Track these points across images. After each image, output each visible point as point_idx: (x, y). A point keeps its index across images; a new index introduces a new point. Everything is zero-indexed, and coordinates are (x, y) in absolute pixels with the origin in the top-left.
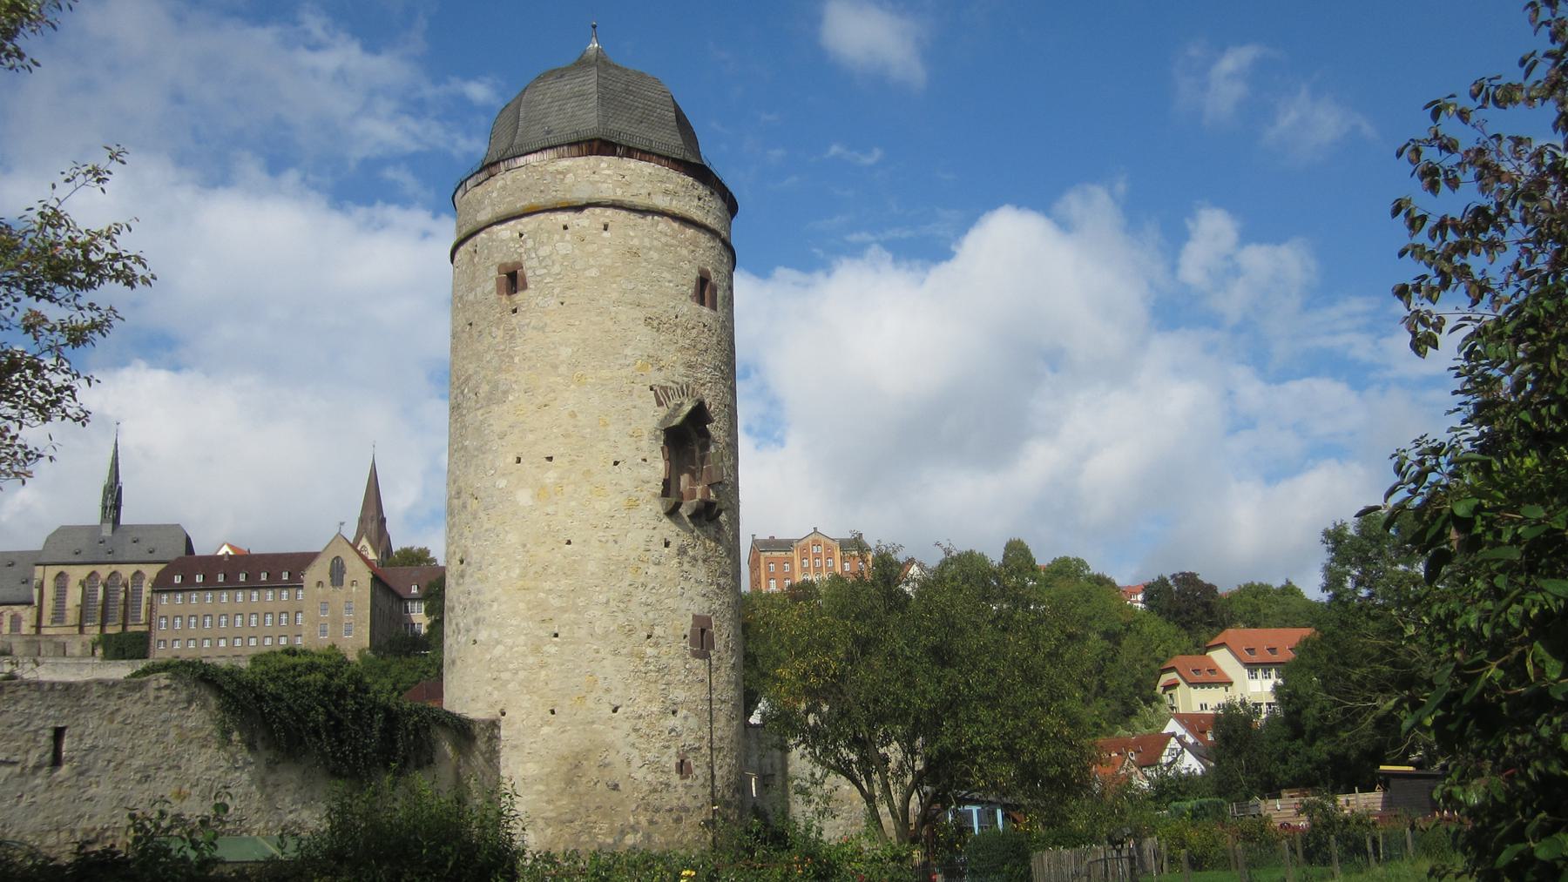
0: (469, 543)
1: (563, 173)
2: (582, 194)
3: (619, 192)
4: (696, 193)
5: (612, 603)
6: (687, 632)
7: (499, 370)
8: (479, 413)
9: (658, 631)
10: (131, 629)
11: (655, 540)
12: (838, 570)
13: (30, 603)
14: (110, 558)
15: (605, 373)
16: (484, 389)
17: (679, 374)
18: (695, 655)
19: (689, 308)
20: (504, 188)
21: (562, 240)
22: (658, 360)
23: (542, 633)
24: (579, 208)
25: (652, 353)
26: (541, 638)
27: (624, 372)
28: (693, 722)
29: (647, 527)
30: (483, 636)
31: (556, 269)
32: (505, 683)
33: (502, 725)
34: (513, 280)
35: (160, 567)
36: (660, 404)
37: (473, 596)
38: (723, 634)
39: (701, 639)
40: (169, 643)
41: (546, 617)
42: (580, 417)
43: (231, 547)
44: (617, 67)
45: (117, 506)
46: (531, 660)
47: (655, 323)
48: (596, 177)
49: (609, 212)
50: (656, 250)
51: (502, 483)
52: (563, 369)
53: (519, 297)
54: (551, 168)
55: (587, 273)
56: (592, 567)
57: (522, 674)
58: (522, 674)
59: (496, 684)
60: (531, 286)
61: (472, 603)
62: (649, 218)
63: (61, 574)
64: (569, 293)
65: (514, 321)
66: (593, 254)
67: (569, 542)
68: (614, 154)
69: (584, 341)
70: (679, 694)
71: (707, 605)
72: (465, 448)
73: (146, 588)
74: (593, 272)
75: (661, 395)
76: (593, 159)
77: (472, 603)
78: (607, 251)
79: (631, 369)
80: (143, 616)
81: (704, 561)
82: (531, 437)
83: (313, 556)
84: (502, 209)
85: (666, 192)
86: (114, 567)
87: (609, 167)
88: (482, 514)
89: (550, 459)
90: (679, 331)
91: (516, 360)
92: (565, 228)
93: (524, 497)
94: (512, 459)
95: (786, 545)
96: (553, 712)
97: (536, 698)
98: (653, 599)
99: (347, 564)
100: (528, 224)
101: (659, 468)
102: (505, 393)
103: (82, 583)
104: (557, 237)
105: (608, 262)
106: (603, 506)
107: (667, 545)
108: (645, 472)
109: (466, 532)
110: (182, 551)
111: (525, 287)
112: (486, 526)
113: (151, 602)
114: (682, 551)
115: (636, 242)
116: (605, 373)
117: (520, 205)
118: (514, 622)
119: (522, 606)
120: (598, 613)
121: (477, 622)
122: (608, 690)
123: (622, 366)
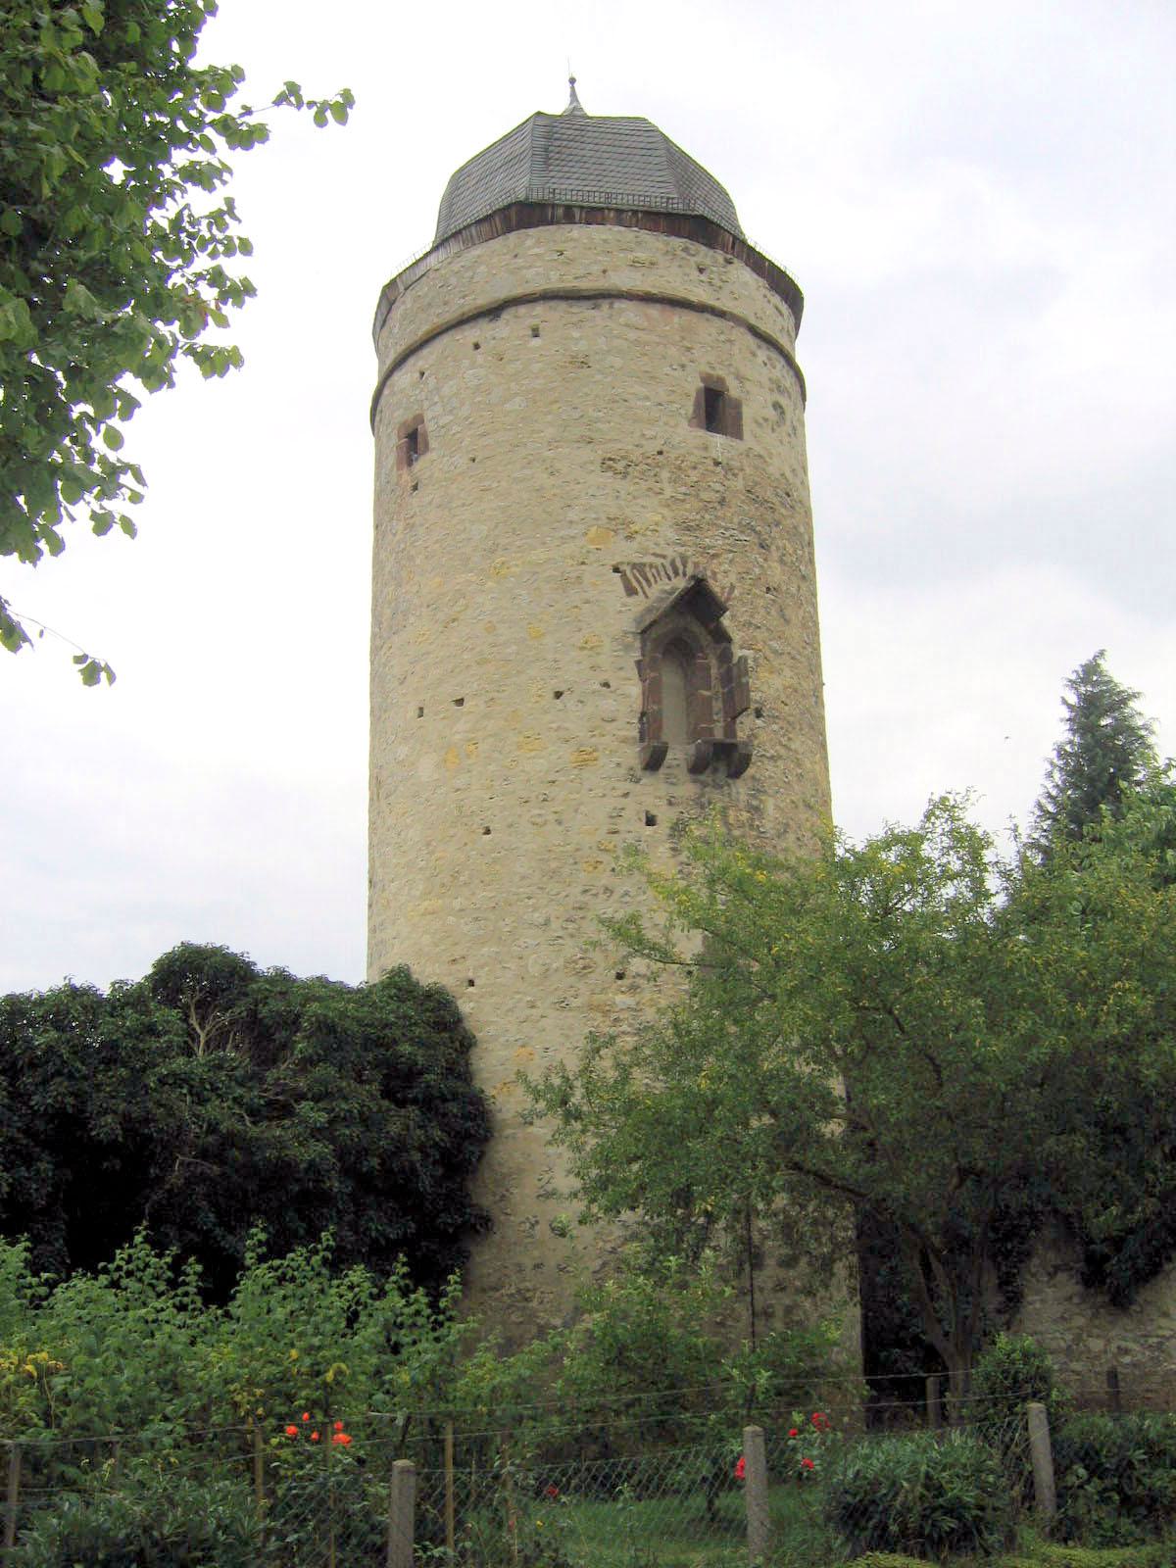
3: (554, 275)
5: (555, 925)
21: (473, 366)
24: (493, 312)
25: (613, 512)
31: (465, 411)
36: (631, 591)
47: (620, 466)
48: (520, 261)
54: (456, 267)
60: (433, 444)
67: (488, 832)
75: (632, 578)
76: (513, 237)
85: (635, 264)
89: (460, 702)
104: (466, 363)
107: (650, 821)
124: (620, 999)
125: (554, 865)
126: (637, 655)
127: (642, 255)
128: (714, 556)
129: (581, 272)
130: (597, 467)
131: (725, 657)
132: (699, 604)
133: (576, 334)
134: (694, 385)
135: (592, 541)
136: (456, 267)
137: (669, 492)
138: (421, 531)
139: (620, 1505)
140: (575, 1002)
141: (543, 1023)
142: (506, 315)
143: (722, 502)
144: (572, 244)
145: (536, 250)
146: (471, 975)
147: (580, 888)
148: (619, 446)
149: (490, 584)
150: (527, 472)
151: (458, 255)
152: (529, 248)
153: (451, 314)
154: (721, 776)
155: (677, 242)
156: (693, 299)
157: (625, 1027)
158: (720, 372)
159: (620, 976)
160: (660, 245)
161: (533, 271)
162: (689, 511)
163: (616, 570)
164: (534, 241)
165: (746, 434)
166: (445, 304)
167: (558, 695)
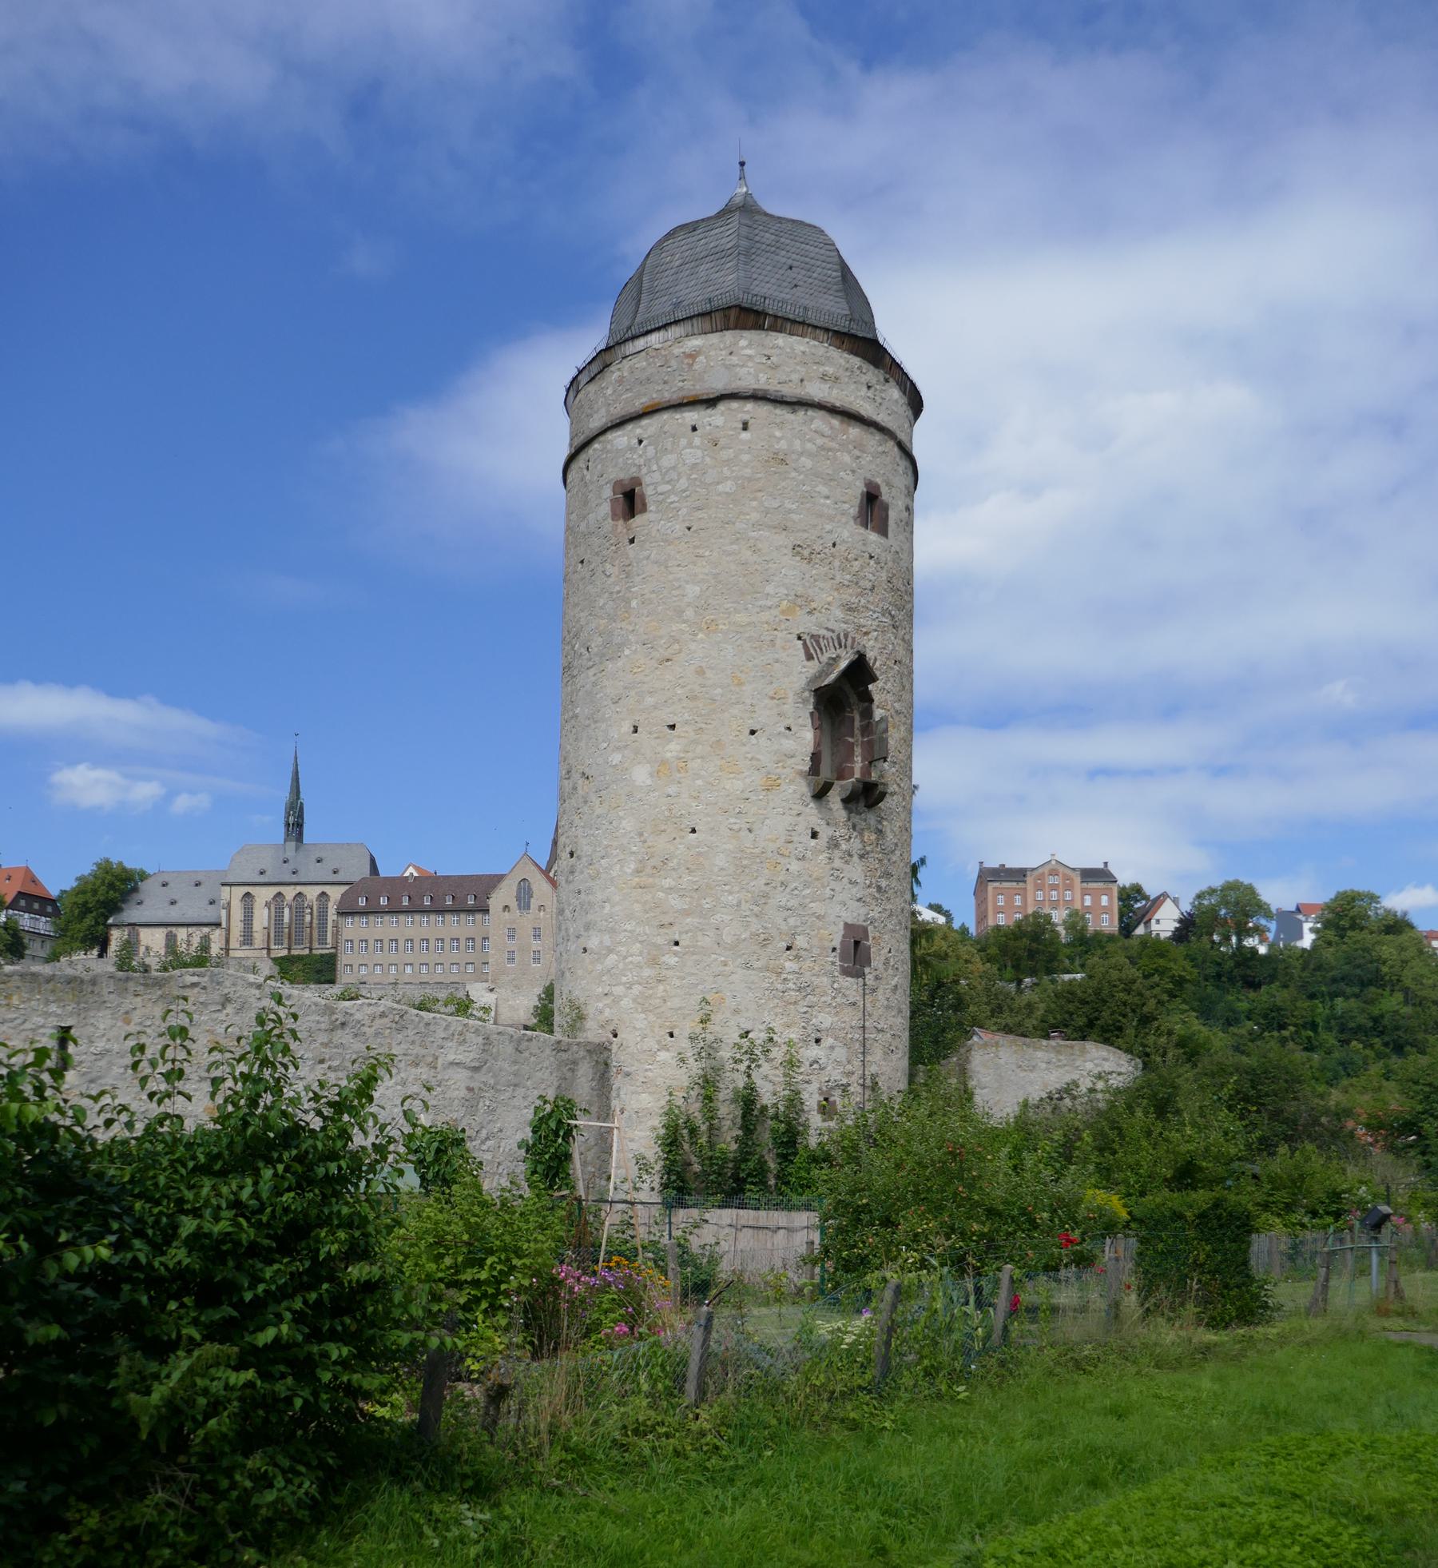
0: (580, 832)
1: (692, 356)
2: (717, 383)
3: (763, 378)
4: (864, 379)
5: (744, 906)
6: (837, 943)
7: (612, 619)
8: (591, 672)
9: (800, 942)
10: (294, 952)
11: (800, 828)
12: (1078, 906)
13: (218, 925)
14: (294, 879)
15: (741, 618)
16: (596, 642)
17: (835, 620)
18: (846, 972)
19: (852, 533)
20: (621, 381)
21: (690, 445)
22: (809, 600)
23: (660, 940)
24: (711, 402)
25: (800, 590)
26: (657, 946)
27: (766, 616)
28: (841, 1053)
29: (788, 811)
30: (593, 943)
31: (683, 483)
32: (617, 1000)
33: (614, 1048)
34: (630, 501)
35: (345, 888)
36: (809, 657)
37: (583, 896)
38: (890, 954)
39: (855, 952)
40: (355, 967)
41: (666, 920)
42: (709, 674)
43: (417, 868)
44: (766, 214)
45: (299, 825)
46: (647, 972)
47: (806, 553)
48: (734, 359)
49: (749, 406)
50: (810, 455)
51: (616, 758)
52: (689, 613)
53: (638, 520)
54: (677, 351)
55: (720, 488)
56: (720, 861)
57: (637, 989)
58: (637, 989)
59: (608, 1000)
60: (651, 507)
61: (582, 904)
62: (801, 413)
63: (248, 894)
64: (699, 514)
65: (631, 554)
66: (728, 462)
67: (694, 831)
68: (761, 327)
69: (716, 576)
70: (825, 1019)
71: (863, 911)
72: (576, 716)
73: (332, 915)
74: (728, 487)
75: (811, 646)
76: (729, 335)
77: (582, 904)
78: (745, 457)
79: (775, 612)
80: (329, 940)
81: (861, 857)
82: (650, 700)
83: (500, 878)
84: (619, 410)
85: (824, 378)
86: (299, 889)
87: (750, 346)
88: (593, 798)
89: (673, 727)
90: (837, 563)
91: (634, 603)
92: (694, 429)
93: (641, 775)
94: (627, 727)
95: (1019, 875)
96: (671, 1035)
97: (652, 1017)
98: (793, 903)
99: (534, 887)
100: (648, 426)
101: (806, 737)
102: (621, 646)
103: (268, 905)
104: (683, 442)
105: (747, 472)
106: (735, 785)
107: (814, 835)
108: (788, 744)
109: (577, 821)
110: (366, 871)
111: (644, 509)
112: (598, 811)
113: (336, 926)
114: (833, 844)
115: (783, 445)
116: (741, 618)
117: (638, 405)
118: (628, 927)
119: (637, 907)
120: (727, 918)
121: (587, 927)
122: (736, 1011)
123: (763, 609)
124: (788, 964)
125: (745, 862)
126: (811, 708)
127: (830, 370)
128: (866, 633)
129: (784, 378)
130: (789, 551)
131: (867, 714)
132: (859, 673)
133: (778, 434)
134: (860, 488)
135: (783, 612)
136: (677, 351)
137: (838, 578)
138: (637, 579)
139: (363, 971)
140: (757, 965)
141: (733, 977)
142: (722, 407)
143: (872, 589)
144: (777, 351)
145: (749, 352)
146: (677, 938)
147: (764, 881)
148: (806, 535)
149: (700, 636)
150: (735, 547)
151: (678, 340)
152: (743, 348)
153: (668, 395)
154: (862, 804)
155: (856, 361)
156: (863, 413)
157: (791, 985)
158: (878, 480)
159: (789, 948)
160: (842, 361)
161: (745, 370)
162: (849, 595)
163: (799, 638)
164: (746, 343)
165: (890, 534)
166: (665, 382)
167: (753, 732)
